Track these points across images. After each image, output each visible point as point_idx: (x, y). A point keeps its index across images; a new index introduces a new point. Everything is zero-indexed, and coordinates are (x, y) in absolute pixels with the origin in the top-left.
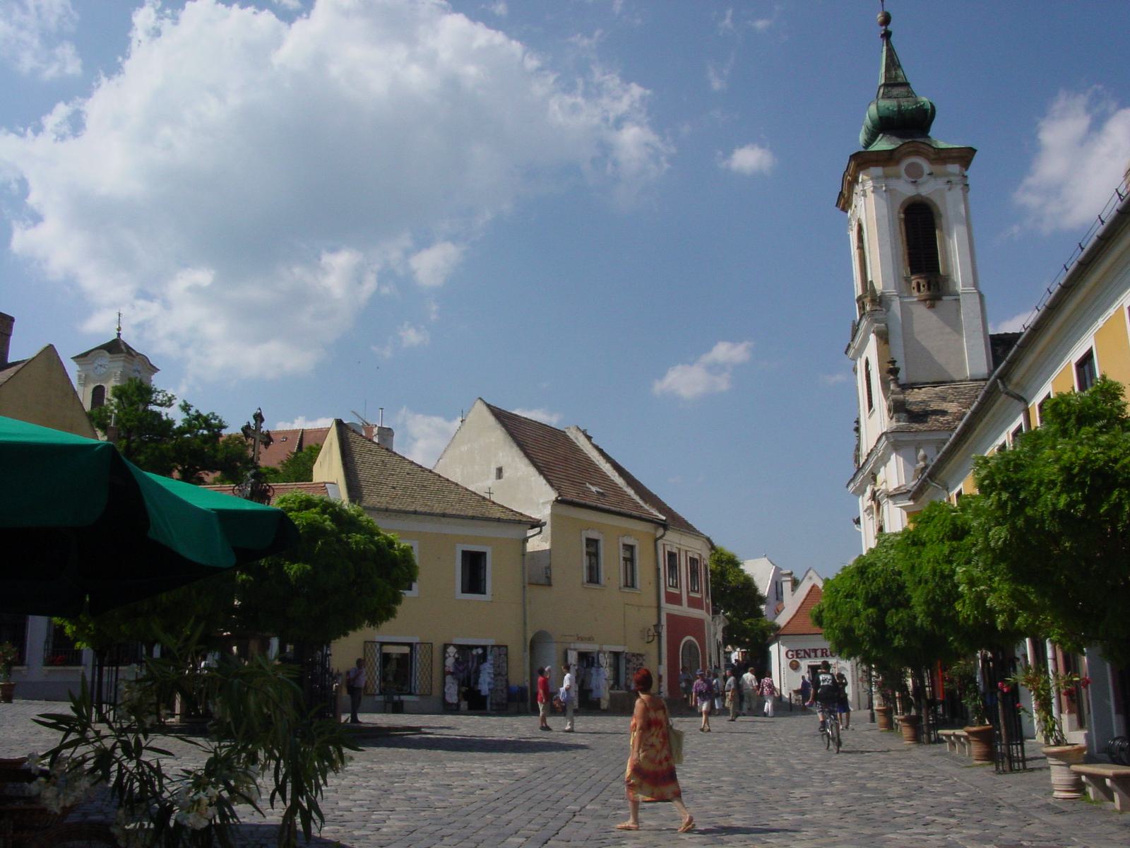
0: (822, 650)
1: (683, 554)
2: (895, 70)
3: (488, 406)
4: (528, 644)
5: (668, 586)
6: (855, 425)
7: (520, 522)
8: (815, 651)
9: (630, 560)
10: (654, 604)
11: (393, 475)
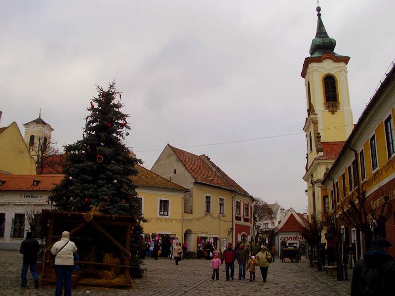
3: (320, 25)
4: (184, 232)
8: (291, 238)
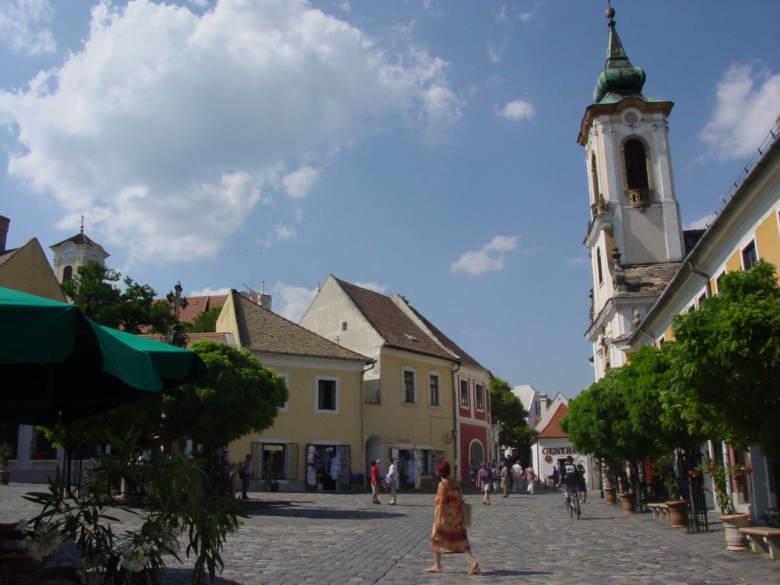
0: (568, 448)
1: (471, 382)
2: (618, 48)
3: (337, 280)
4: (365, 444)
5: (461, 404)
6: (590, 293)
7: (359, 360)
8: (563, 449)
9: (435, 387)
10: (452, 416)
11: (271, 327)
